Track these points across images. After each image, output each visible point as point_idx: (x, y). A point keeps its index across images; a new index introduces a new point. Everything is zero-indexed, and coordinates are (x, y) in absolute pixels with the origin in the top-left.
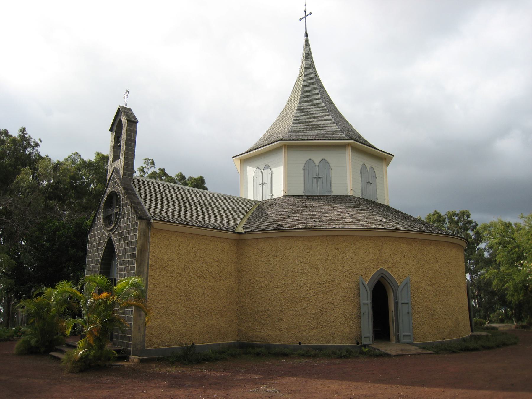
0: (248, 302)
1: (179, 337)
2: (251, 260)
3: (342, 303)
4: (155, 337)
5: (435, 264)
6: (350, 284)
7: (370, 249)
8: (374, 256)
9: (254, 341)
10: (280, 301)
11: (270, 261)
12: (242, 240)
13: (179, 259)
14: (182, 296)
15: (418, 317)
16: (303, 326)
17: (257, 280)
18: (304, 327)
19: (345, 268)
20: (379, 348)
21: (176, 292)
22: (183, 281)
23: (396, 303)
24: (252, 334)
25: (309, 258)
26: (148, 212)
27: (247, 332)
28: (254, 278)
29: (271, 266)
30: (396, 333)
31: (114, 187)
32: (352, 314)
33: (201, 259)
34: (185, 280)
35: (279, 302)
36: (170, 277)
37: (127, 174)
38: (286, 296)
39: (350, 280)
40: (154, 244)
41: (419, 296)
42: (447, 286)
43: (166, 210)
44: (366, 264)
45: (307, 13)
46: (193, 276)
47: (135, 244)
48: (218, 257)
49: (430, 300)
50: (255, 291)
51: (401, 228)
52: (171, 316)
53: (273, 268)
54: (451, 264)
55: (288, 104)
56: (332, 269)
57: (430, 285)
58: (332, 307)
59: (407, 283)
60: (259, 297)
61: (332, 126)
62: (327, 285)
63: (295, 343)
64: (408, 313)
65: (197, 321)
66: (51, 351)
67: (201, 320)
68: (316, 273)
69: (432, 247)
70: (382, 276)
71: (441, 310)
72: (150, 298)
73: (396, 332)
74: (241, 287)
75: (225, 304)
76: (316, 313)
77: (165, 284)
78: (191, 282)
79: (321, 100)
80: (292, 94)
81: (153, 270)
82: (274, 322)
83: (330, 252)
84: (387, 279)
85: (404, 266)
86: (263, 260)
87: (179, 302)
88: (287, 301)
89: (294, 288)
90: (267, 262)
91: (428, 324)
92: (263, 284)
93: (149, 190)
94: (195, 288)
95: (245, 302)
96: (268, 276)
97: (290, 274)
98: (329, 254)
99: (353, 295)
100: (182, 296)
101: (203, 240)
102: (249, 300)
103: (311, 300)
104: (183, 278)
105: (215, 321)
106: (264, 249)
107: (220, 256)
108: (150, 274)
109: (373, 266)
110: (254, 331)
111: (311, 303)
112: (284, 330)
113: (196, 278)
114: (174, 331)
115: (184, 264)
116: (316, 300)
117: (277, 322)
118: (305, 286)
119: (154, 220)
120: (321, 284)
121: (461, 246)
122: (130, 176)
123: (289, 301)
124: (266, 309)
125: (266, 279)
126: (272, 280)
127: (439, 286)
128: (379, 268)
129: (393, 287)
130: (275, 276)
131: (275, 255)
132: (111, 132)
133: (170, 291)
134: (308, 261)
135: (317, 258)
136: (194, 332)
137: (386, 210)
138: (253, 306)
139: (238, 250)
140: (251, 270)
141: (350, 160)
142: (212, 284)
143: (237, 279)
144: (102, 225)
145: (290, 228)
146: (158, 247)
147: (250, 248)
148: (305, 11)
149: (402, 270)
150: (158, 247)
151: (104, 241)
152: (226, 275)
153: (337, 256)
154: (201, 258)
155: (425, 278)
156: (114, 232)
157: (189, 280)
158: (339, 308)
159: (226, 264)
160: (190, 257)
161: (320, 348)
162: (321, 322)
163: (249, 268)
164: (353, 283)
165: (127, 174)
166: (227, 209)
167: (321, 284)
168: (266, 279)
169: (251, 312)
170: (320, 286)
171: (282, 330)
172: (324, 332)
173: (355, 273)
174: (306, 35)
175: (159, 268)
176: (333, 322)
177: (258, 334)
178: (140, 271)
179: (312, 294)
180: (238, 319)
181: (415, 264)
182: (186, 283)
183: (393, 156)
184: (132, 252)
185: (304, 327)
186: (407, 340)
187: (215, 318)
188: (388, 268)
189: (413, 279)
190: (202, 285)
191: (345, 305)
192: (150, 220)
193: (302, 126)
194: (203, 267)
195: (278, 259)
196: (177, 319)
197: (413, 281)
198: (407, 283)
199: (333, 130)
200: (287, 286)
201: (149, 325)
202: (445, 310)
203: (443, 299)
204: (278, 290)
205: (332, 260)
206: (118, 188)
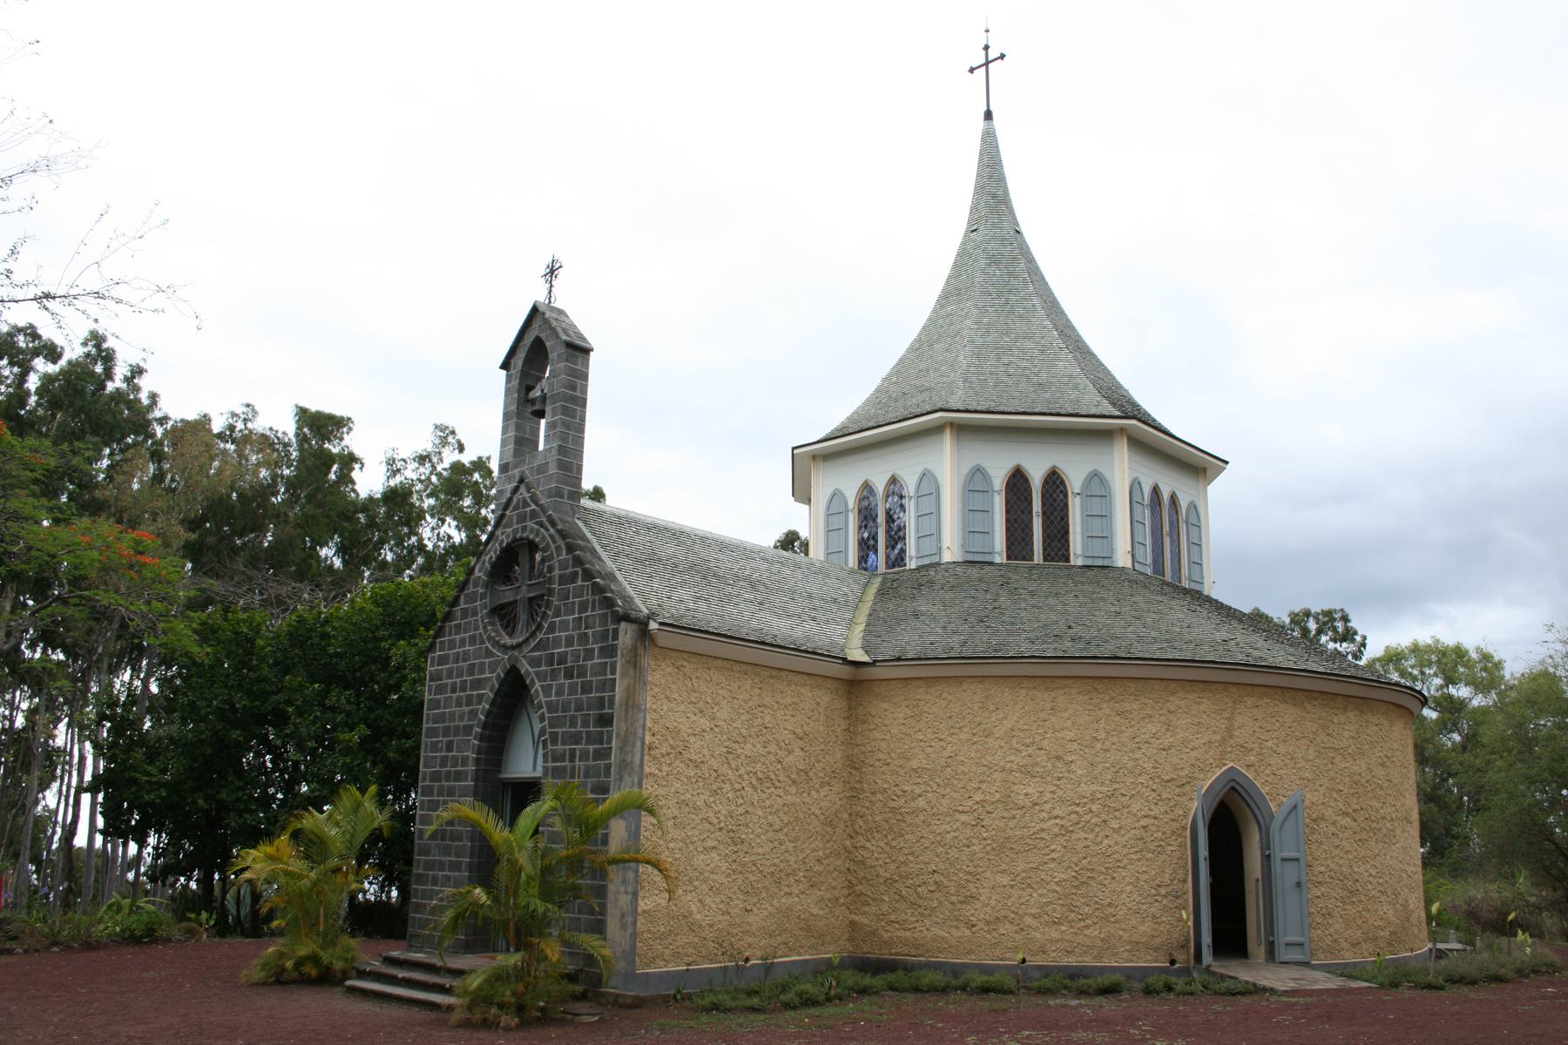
0: (880, 850)
1: (713, 941)
2: (888, 737)
3: (1133, 856)
4: (658, 941)
5: (1356, 757)
6: (1153, 807)
7: (1205, 716)
8: (1214, 732)
9: (897, 954)
10: (968, 847)
11: (941, 740)
12: (862, 681)
13: (715, 729)
14: (721, 829)
15: (1318, 897)
16: (1031, 914)
17: (904, 792)
18: (1034, 916)
19: (1141, 762)
20: (1232, 974)
21: (707, 820)
22: (724, 791)
23: (1267, 859)
24: (890, 934)
25: (1048, 736)
26: (638, 602)
27: (877, 930)
28: (897, 785)
29: (946, 754)
30: (1266, 937)
31: (524, 529)
32: (1159, 886)
33: (765, 731)
34: (727, 787)
35: (965, 849)
36: (694, 780)
37: (566, 492)
38: (985, 835)
39: (1153, 794)
40: (657, 690)
41: (1321, 843)
42: (1384, 818)
43: (675, 596)
44: (1194, 754)
45: (993, 54)
46: (746, 777)
47: (607, 687)
48: (805, 727)
49: (1347, 852)
50: (899, 820)
51: (1321, 669)
52: (696, 883)
53: (949, 760)
54: (1393, 759)
55: (942, 306)
56: (1107, 765)
57: (1346, 814)
58: (1107, 865)
59: (1296, 806)
60: (910, 836)
61: (1071, 377)
62: (1094, 808)
63: (1009, 959)
64: (1299, 884)
65: (756, 900)
66: (347, 979)
67: (764, 894)
68: (1067, 775)
69: (1351, 715)
70: (1233, 788)
71: (1371, 879)
72: (647, 834)
73: (1266, 933)
74: (859, 808)
75: (820, 853)
76: (1065, 880)
77: (683, 798)
78: (742, 792)
79: (1036, 301)
80: (950, 277)
81: (654, 758)
82: (952, 903)
83: (1102, 721)
84: (1247, 798)
85: (1287, 761)
86: (921, 737)
87: (714, 848)
88: (988, 848)
89: (1006, 815)
90: (933, 744)
91: (1341, 916)
92: (921, 803)
93: (619, 538)
94: (750, 810)
95: (871, 848)
96: (938, 780)
97: (997, 776)
98: (1101, 726)
99: (1160, 834)
100: (721, 829)
101: (772, 681)
102: (882, 844)
103: (1053, 847)
104: (723, 781)
105: (797, 899)
106: (926, 709)
107: (808, 724)
108: (647, 770)
109: (1212, 761)
110: (897, 926)
111: (1053, 855)
112: (981, 925)
113: (754, 782)
114: (704, 924)
115: (726, 744)
116: (1065, 847)
117: (961, 902)
118: (1037, 808)
119: (661, 624)
120: (1078, 805)
121: (1404, 707)
122: (573, 500)
123: (993, 849)
124: (930, 870)
125: (929, 789)
126: (948, 790)
127: (1367, 816)
128: (1225, 765)
129: (1260, 818)
130: (955, 782)
131: (958, 726)
132: (504, 372)
133: (693, 816)
134: (1046, 742)
135: (1071, 735)
136: (748, 928)
137: (1227, 613)
138: (894, 861)
139: (850, 708)
140: (888, 764)
141: (1124, 472)
142: (790, 799)
143: (848, 786)
144: (481, 631)
145: (999, 654)
146: (667, 697)
147: (885, 705)
148: (986, 48)
149: (1281, 771)
150: (667, 697)
151: (493, 677)
152: (822, 775)
153: (1121, 732)
154: (766, 728)
155: (1335, 795)
156: (531, 651)
157: (737, 786)
158: (1124, 868)
159: (822, 747)
160: (740, 726)
161: (1074, 974)
162: (1078, 904)
163: (881, 756)
164: (1160, 803)
165: (566, 492)
166: (810, 597)
167: (1078, 805)
168: (929, 789)
169: (888, 875)
170: (1078, 809)
171: (973, 926)
172: (1086, 932)
173: (1166, 778)
174: (988, 115)
175: (668, 754)
176: (1110, 905)
177: (908, 934)
178: (624, 761)
179: (1056, 830)
180: (849, 895)
181: (1311, 757)
182: (730, 795)
183: (1227, 463)
184: (599, 709)
185: (1034, 916)
186: (1294, 955)
187: (797, 892)
188: (1248, 766)
189: (1308, 796)
190: (767, 801)
191: (1139, 860)
192: (647, 624)
193: (991, 373)
194: (770, 753)
195: (964, 736)
196: (711, 893)
197: (1307, 803)
198: (1296, 806)
199: (1076, 387)
200: (989, 809)
201: (646, 908)
202: (1381, 881)
203: (1377, 851)
204: (964, 818)
205: (1107, 743)
206: (542, 530)
